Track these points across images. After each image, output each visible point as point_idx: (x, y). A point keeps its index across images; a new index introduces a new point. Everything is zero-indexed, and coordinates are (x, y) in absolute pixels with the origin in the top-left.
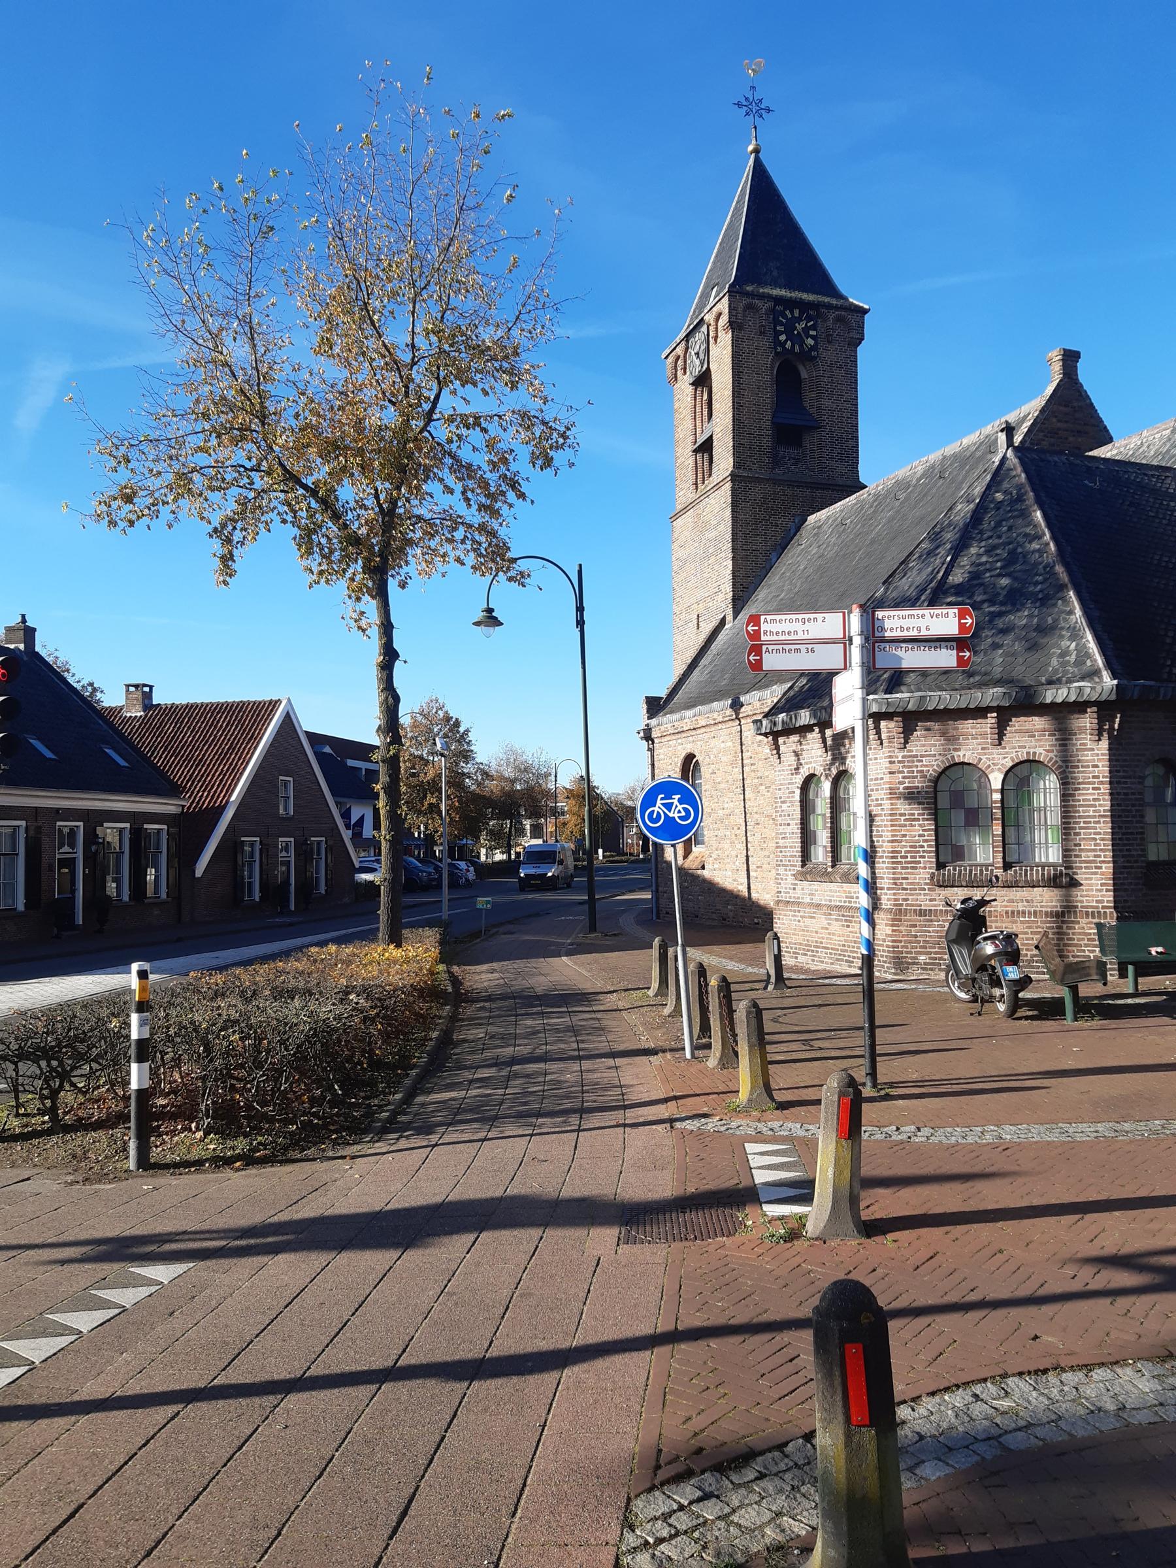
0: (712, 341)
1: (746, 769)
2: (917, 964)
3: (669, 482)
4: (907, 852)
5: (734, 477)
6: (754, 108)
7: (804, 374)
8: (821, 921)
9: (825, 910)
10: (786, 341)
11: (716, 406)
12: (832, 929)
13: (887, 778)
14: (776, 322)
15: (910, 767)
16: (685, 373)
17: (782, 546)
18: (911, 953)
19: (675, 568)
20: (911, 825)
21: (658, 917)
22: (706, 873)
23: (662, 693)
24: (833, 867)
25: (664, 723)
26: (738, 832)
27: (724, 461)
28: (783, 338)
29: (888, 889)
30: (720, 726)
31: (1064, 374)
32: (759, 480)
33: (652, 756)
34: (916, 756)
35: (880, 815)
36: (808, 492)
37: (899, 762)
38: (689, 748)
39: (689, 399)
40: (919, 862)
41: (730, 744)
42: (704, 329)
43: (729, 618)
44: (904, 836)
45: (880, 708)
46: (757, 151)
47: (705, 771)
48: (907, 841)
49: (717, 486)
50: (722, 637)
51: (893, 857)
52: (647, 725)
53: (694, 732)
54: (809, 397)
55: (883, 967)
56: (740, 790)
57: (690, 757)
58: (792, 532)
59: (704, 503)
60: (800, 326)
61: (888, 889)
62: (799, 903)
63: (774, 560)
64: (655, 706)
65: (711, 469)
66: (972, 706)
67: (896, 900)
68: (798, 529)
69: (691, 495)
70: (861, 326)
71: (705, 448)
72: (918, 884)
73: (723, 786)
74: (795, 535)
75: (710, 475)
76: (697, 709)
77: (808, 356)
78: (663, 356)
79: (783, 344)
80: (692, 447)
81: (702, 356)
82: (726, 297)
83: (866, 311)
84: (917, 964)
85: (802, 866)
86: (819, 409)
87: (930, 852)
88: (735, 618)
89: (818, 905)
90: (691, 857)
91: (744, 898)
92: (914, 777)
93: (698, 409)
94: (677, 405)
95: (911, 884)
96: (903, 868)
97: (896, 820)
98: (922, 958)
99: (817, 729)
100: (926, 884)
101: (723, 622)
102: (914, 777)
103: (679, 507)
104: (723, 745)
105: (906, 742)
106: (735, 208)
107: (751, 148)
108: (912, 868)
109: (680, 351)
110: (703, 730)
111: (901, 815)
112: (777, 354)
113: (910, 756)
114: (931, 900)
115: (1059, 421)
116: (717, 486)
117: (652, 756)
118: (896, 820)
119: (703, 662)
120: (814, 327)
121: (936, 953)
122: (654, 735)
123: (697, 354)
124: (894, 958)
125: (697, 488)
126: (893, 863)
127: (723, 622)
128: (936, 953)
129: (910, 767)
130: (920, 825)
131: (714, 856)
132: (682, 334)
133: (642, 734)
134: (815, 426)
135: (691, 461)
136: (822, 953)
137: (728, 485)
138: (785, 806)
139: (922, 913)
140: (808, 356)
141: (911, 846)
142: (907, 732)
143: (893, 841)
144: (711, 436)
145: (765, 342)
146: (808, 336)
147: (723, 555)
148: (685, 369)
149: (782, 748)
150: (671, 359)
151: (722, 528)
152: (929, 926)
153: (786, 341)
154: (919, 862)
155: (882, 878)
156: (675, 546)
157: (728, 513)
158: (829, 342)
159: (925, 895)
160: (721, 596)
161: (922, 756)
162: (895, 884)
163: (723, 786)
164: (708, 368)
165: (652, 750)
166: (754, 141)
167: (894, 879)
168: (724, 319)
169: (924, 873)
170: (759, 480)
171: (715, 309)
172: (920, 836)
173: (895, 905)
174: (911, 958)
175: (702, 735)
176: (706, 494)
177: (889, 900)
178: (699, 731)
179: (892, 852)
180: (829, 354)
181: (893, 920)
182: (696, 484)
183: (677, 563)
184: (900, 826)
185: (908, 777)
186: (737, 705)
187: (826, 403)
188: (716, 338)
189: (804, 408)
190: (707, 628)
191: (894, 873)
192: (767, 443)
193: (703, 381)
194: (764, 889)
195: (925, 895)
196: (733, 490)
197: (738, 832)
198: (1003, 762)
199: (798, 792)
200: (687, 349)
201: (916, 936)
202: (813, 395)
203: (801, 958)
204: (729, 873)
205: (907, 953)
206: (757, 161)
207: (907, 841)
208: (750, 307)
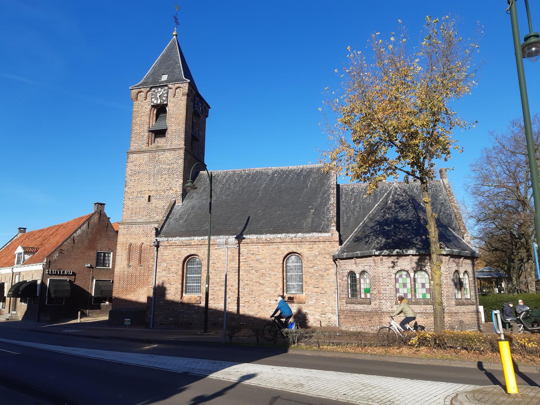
1: (241, 263)
39: (148, 110)
78: (130, 88)
139: (456, 313)
156: (130, 164)
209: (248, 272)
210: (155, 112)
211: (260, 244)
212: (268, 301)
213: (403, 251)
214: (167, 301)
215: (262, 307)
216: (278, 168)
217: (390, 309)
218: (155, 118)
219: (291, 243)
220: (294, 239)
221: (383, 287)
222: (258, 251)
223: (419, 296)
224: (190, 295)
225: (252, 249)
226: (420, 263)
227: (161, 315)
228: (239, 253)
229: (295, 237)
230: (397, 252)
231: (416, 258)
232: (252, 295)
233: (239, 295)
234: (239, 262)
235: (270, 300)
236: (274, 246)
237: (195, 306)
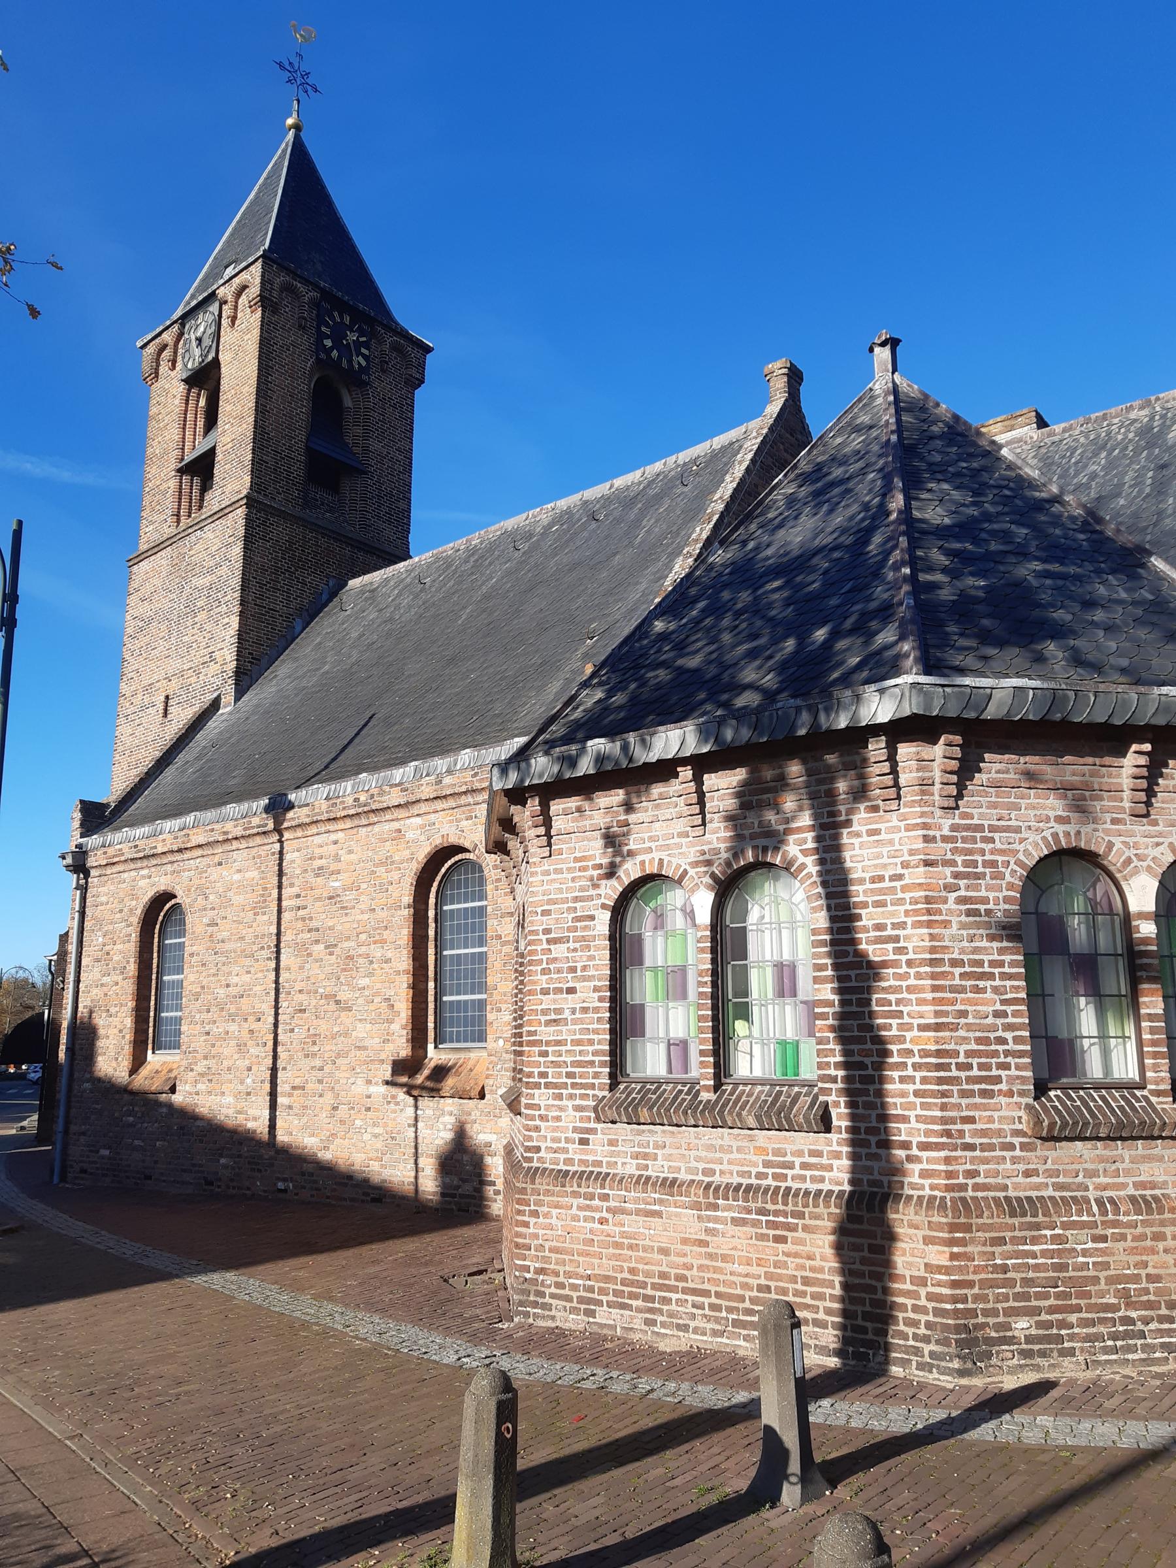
0: (225, 322)
1: (286, 916)
2: (1011, 1341)
3: (130, 507)
4: (970, 1054)
5: (251, 502)
6: (298, 78)
7: (348, 402)
8: (683, 1219)
9: (697, 1195)
10: (332, 348)
11: (224, 408)
12: (720, 1245)
13: (918, 874)
14: (321, 322)
15: (970, 852)
16: (173, 368)
17: (312, 611)
18: (994, 1313)
19: (129, 631)
20: (977, 990)
21: (63, 1179)
22: (177, 1099)
23: (110, 793)
24: (717, 1087)
25: (119, 841)
26: (255, 1026)
27: (233, 479)
28: (328, 343)
29: (924, 1147)
30: (235, 844)
31: (789, 394)
32: (281, 514)
33: (84, 899)
34: (979, 828)
35: (895, 964)
36: (347, 551)
37: (945, 839)
38: (162, 883)
39: (178, 401)
40: (997, 1080)
41: (254, 874)
42: (214, 308)
43: (228, 698)
44: (963, 1014)
45: (928, 702)
46: (297, 127)
47: (195, 922)
48: (969, 1027)
49: (221, 514)
50: (214, 725)
51: (939, 1067)
52: (79, 846)
53: (178, 857)
54: (353, 433)
55: (917, 1352)
56: (269, 953)
57: (163, 897)
58: (325, 597)
59: (193, 538)
60: (352, 337)
61: (924, 1147)
62: (602, 1178)
63: (298, 629)
64: (96, 817)
65: (202, 500)
66: (1118, 722)
67: (950, 1175)
68: (334, 594)
69: (168, 530)
70: (422, 366)
71: (201, 470)
72: (999, 1133)
73: (228, 946)
74: (330, 600)
75: (201, 507)
76: (190, 819)
77: (357, 380)
78: (139, 344)
79: (328, 351)
80: (173, 465)
81: (207, 342)
82: (259, 264)
83: (428, 350)
84: (1011, 1341)
85: (613, 1087)
86: (366, 450)
87: (1021, 1054)
88: (237, 699)
89: (670, 1185)
90: (144, 1072)
91: (259, 1143)
92: (978, 876)
93: (190, 416)
94: (153, 411)
95: (984, 1133)
96: (964, 1094)
97: (943, 975)
98: (1022, 1326)
99: (686, 773)
100: (1017, 1133)
101: (215, 705)
102: (978, 876)
103: (143, 547)
104: (237, 877)
105: (959, 796)
106: (276, 163)
107: (290, 121)
108: (984, 1093)
109: (167, 337)
110: (199, 852)
111: (955, 963)
112: (319, 361)
113: (968, 828)
114: (1028, 1174)
115: (786, 451)
116: (221, 514)
117: (84, 899)
118: (943, 975)
119: (181, 759)
120: (366, 345)
121: (1052, 1310)
122: (91, 862)
123: (199, 340)
124: (958, 1329)
125: (178, 521)
126: (940, 1081)
127: (215, 705)
128: (1052, 1310)
129: (970, 852)
130: (995, 990)
131: (200, 1068)
132: (179, 313)
133: (69, 860)
134: (358, 471)
135: (173, 484)
136: (680, 1304)
137: (241, 512)
138: (559, 950)
139: (1014, 1207)
140: (357, 380)
141: (979, 1041)
142: (966, 770)
143: (938, 1027)
144: (214, 447)
145: (305, 341)
146: (359, 354)
147: (224, 609)
148: (174, 362)
149: (558, 824)
150: (151, 349)
151: (224, 571)
152: (1035, 1241)
153: (332, 348)
154: (997, 1080)
155: (905, 1119)
156: (133, 600)
157: (237, 550)
158: (384, 371)
159: (1015, 1160)
160: (214, 668)
161: (993, 829)
162: (948, 1134)
163: (228, 946)
164: (216, 363)
165: (84, 889)
166: (295, 115)
167: (944, 1121)
168: (254, 290)
169: (1010, 1112)
170: (281, 514)
171: (237, 280)
172: (998, 1014)
173: (949, 1188)
174: (999, 1327)
175: (192, 863)
176: (199, 526)
177: (924, 1174)
178: (187, 855)
179: (939, 1053)
180: (382, 385)
181: (953, 1228)
182: (178, 515)
183: (132, 623)
184: (953, 989)
185: (967, 876)
186: (279, 807)
187: (375, 445)
188: (234, 319)
189: (347, 444)
190: (182, 716)
191: (943, 1107)
192: (298, 470)
193: (205, 378)
194: (304, 1128)
195: (1015, 1160)
196: (249, 520)
197: (255, 1026)
198: (1156, 852)
199: (604, 918)
200: (181, 334)
201: (1005, 1269)
202: (359, 431)
203: (604, 1316)
204: (229, 1099)
205: (986, 1313)
206: (297, 138)
207: (969, 1027)
208: (287, 288)
209: (303, 950)
210: (202, 403)
211: (340, 825)
212: (360, 1088)
213: (625, 748)
214: (99, 1080)
215: (343, 1111)
216: (573, 500)
217: (574, 1151)
218: (201, 423)
219: (439, 805)
220: (447, 780)
221: (547, 1002)
222: (337, 858)
223: (751, 1061)
224: (169, 1058)
225: (318, 851)
226: (752, 819)
227: (84, 1134)
228: (281, 874)
229: (449, 772)
230: (600, 759)
231: (723, 785)
232: (314, 1055)
233: (275, 1057)
234: (279, 912)
235: (369, 1082)
236: (385, 827)
237: (160, 1104)
